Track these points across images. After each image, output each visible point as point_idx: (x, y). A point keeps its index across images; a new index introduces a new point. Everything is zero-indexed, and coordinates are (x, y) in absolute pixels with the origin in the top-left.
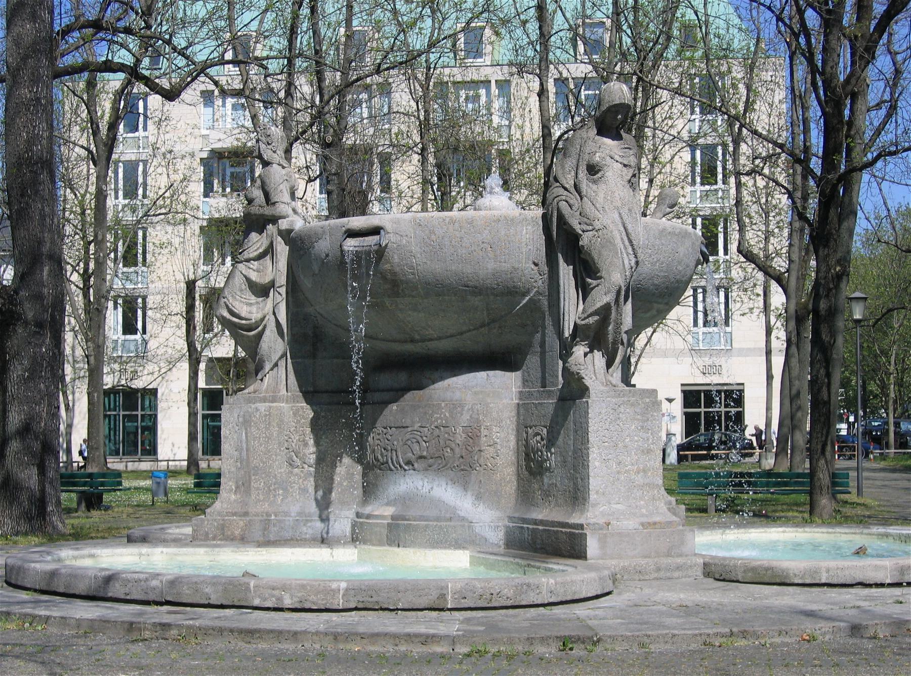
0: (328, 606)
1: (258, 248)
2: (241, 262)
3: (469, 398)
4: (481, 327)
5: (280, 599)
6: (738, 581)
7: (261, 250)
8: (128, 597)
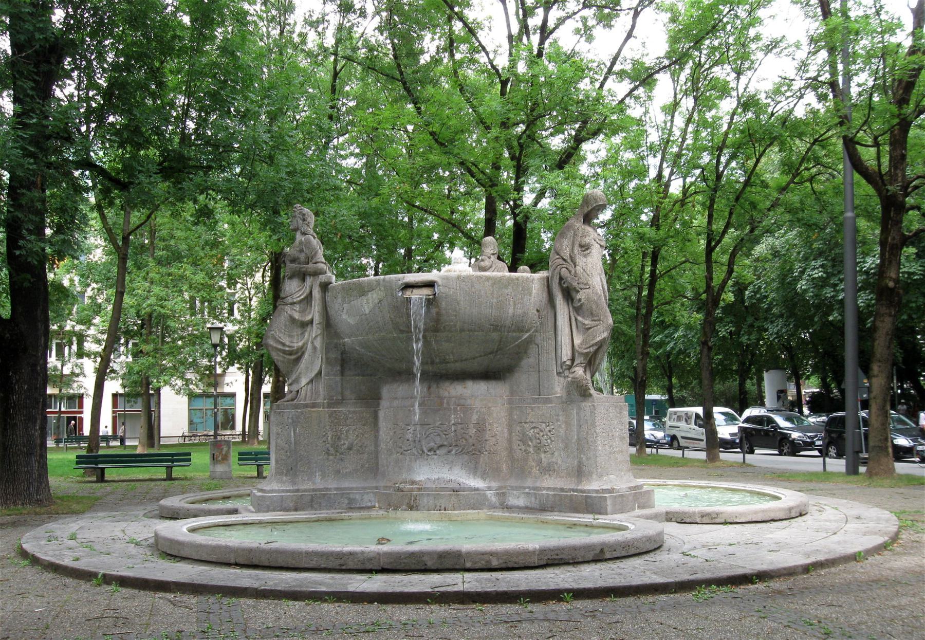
0: (527, 565)
1: (300, 296)
2: (287, 305)
3: (477, 404)
4: (490, 353)
5: (489, 562)
6: (697, 523)
7: (302, 297)
8: (344, 567)
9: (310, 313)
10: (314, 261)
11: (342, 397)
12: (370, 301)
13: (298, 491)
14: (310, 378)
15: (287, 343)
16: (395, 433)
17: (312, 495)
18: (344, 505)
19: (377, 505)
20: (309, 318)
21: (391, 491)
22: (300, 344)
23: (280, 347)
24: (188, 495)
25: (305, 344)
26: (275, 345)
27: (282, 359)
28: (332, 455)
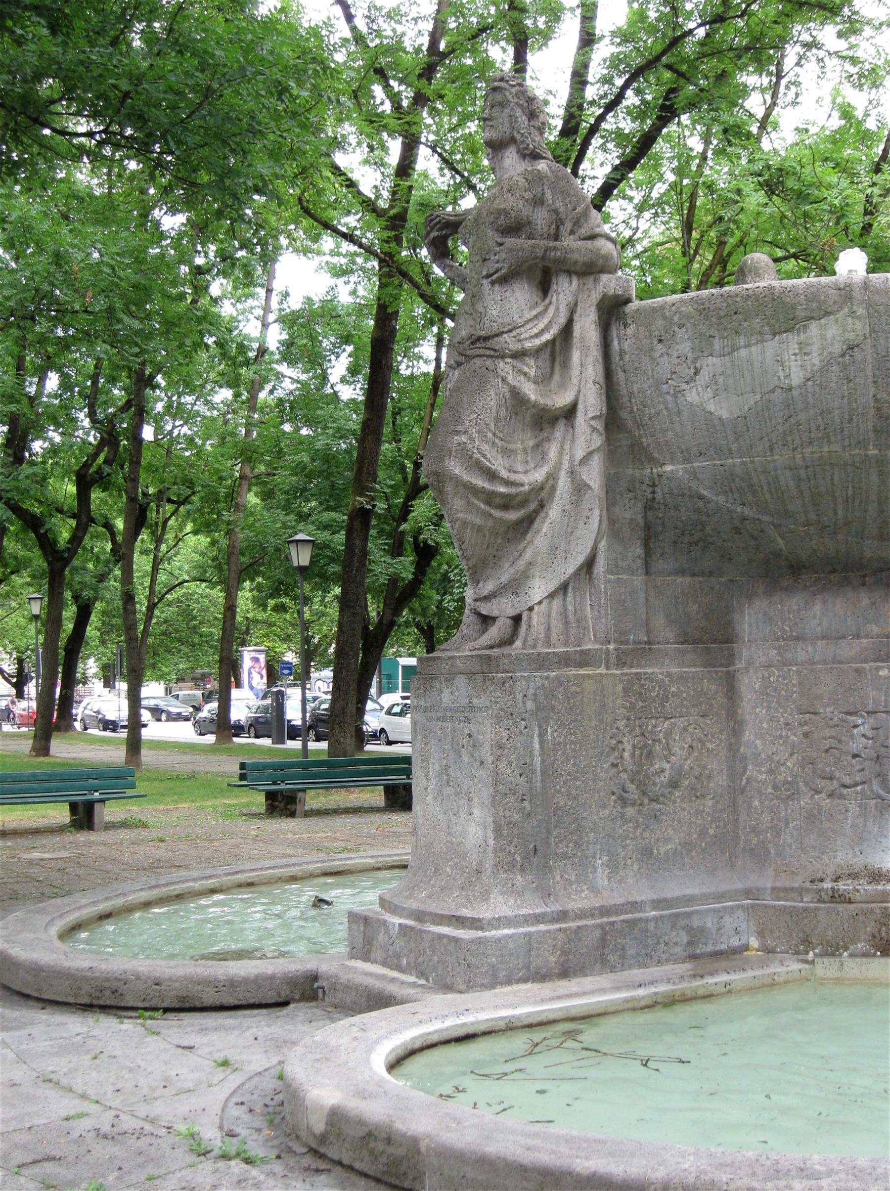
1: (542, 332)
2: (503, 357)
9: (563, 386)
10: (583, 232)
11: (648, 633)
12: (815, 348)
13: (563, 916)
14: (564, 578)
15: (504, 474)
16: (806, 735)
17: (601, 926)
18: (678, 950)
19: (754, 943)
20: (562, 400)
21: (807, 902)
22: (538, 476)
23: (480, 482)
24: (655, 971)
25: (552, 477)
26: (466, 477)
27: (478, 521)
28: (633, 804)
